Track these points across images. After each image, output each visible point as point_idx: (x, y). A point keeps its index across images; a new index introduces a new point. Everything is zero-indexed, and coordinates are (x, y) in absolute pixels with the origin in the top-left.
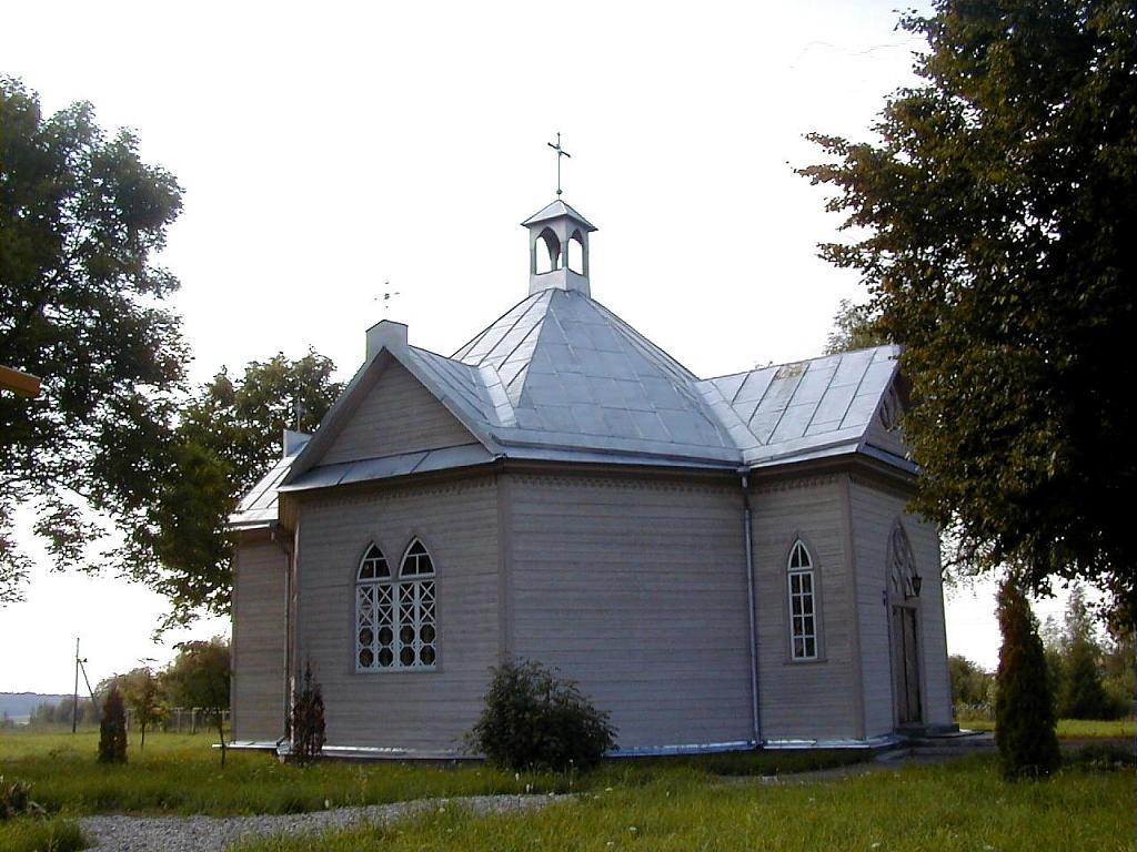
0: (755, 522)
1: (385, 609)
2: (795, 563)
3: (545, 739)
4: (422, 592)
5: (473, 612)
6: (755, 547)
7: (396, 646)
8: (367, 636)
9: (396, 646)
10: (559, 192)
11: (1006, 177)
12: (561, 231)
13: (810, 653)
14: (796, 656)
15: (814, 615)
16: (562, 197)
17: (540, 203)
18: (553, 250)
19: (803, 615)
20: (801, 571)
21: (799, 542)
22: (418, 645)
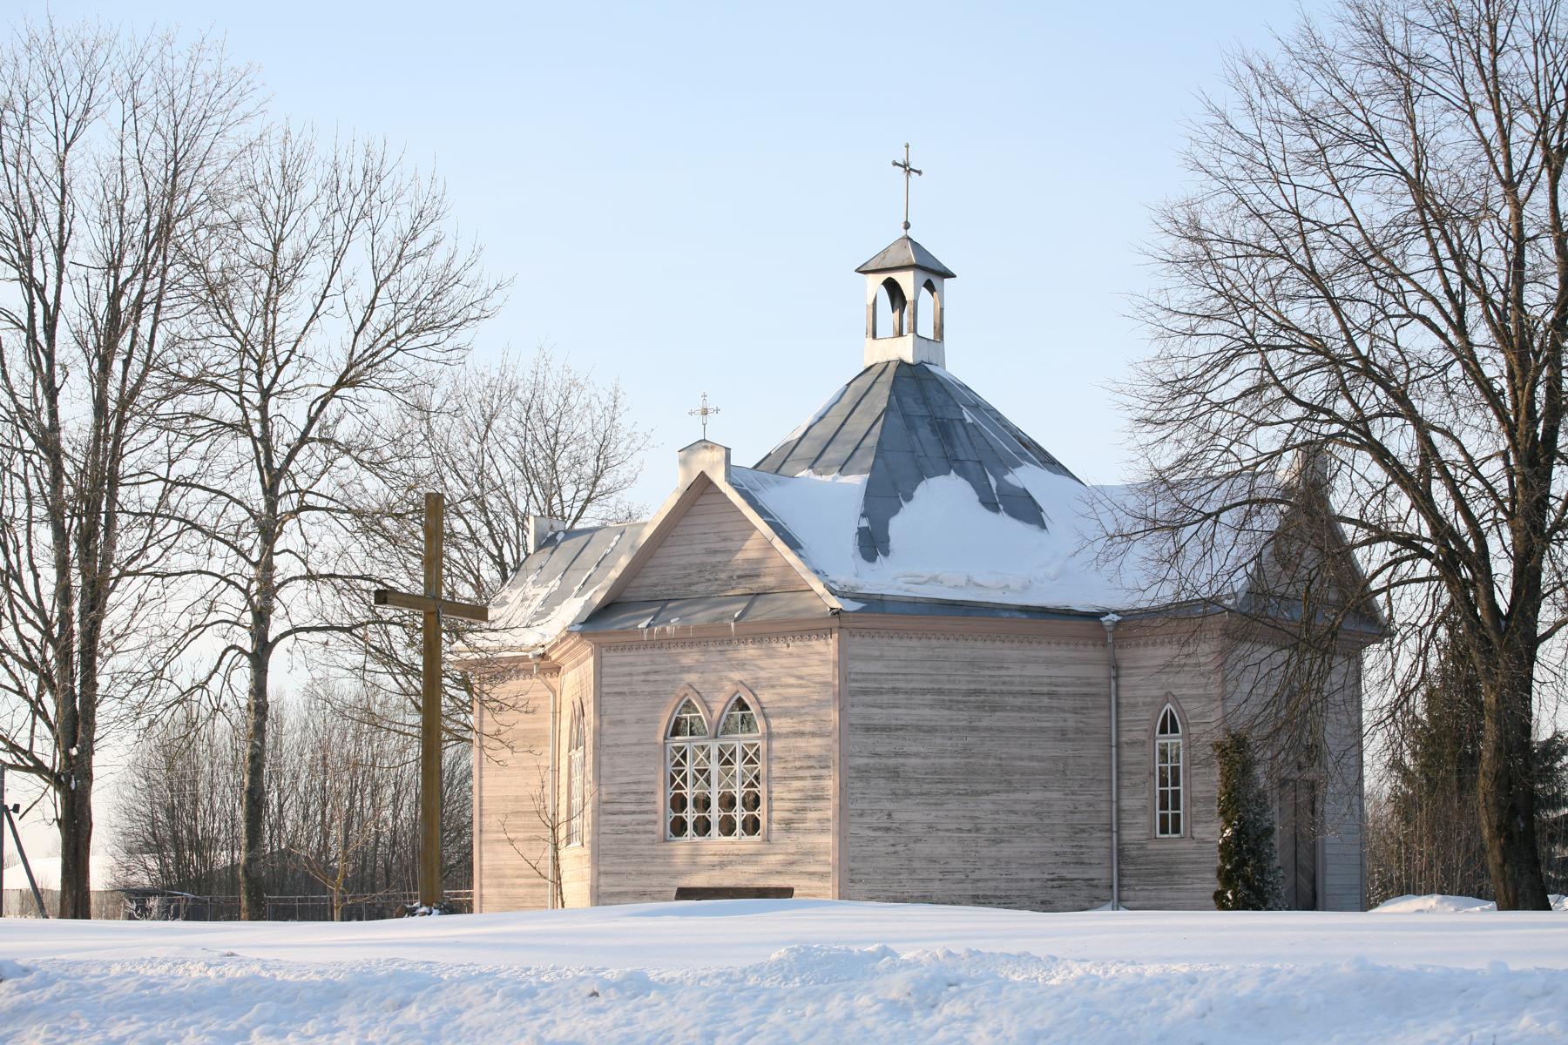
0: (1122, 681)
1: (679, 787)
2: (1163, 731)
3: (1362, 535)
4: (684, 780)
5: (648, 874)
6: (1122, 710)
7: (715, 814)
8: (679, 803)
9: (715, 814)
10: (907, 226)
11: (375, 451)
12: (906, 280)
13: (1176, 830)
14: (1162, 832)
15: (1181, 788)
16: (910, 233)
17: (880, 238)
18: (897, 302)
19: (1170, 788)
20: (1169, 739)
21: (1169, 706)
22: (739, 814)
